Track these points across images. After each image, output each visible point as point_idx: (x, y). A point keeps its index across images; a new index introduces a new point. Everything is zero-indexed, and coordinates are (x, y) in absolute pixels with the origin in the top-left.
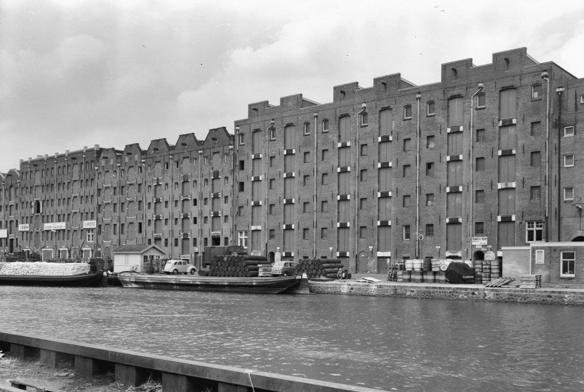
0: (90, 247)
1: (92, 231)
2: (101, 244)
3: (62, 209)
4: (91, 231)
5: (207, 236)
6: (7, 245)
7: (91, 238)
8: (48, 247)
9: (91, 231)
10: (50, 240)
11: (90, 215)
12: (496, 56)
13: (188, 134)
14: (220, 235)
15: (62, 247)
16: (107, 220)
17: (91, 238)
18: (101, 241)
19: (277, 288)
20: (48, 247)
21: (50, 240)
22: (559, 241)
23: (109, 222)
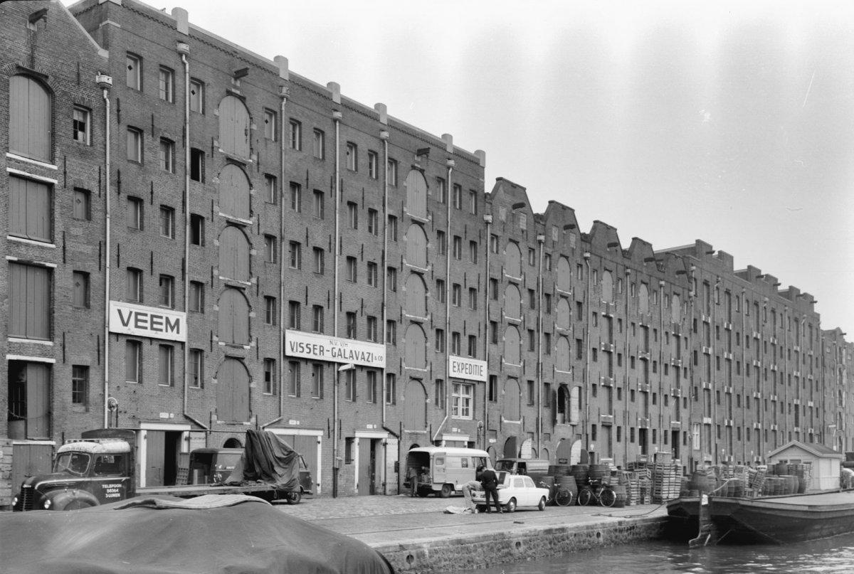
0: (465, 432)
1: (467, 388)
2: (498, 429)
3: (359, 294)
4: (461, 388)
5: (667, 428)
6: (632, 440)
7: (460, 407)
8: (293, 422)
9: (461, 388)
10: (307, 395)
11: (465, 341)
12: (819, 315)
13: (647, 243)
14: (612, 421)
15: (365, 429)
16: (512, 365)
17: (460, 407)
18: (497, 419)
19: (651, 559)
20: (293, 422)
21: (307, 395)
22: (26, 438)
23: (516, 373)
